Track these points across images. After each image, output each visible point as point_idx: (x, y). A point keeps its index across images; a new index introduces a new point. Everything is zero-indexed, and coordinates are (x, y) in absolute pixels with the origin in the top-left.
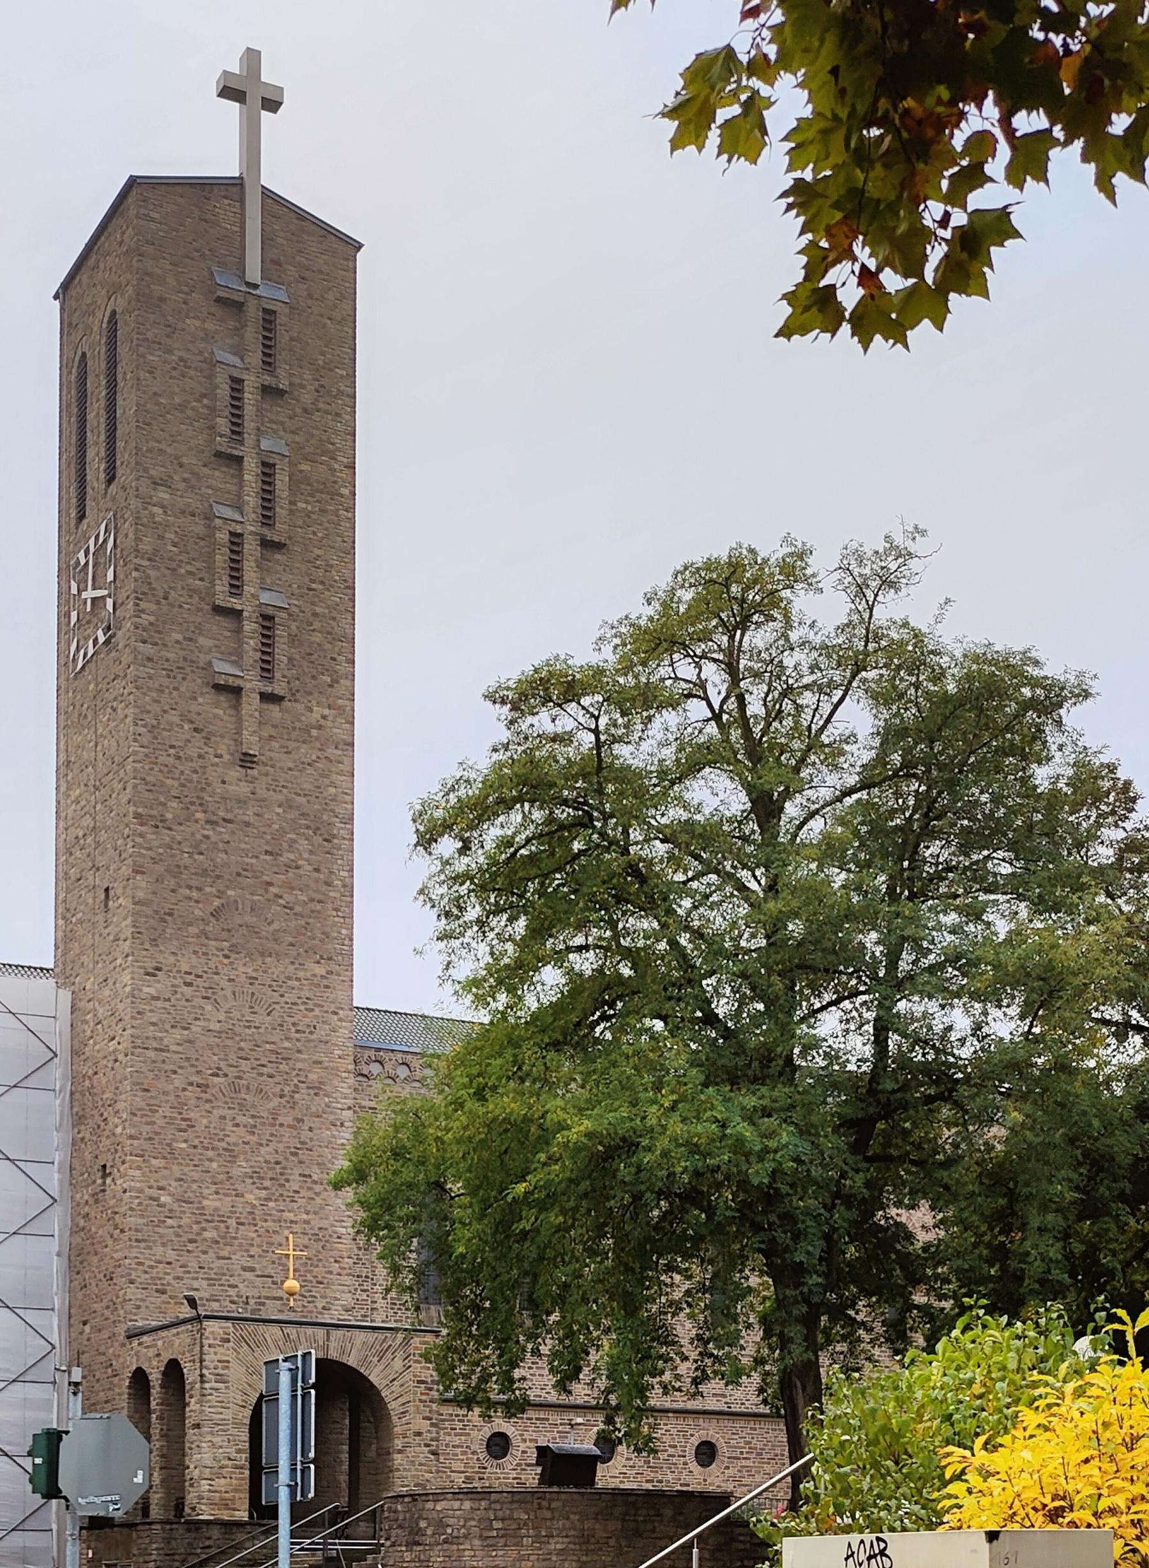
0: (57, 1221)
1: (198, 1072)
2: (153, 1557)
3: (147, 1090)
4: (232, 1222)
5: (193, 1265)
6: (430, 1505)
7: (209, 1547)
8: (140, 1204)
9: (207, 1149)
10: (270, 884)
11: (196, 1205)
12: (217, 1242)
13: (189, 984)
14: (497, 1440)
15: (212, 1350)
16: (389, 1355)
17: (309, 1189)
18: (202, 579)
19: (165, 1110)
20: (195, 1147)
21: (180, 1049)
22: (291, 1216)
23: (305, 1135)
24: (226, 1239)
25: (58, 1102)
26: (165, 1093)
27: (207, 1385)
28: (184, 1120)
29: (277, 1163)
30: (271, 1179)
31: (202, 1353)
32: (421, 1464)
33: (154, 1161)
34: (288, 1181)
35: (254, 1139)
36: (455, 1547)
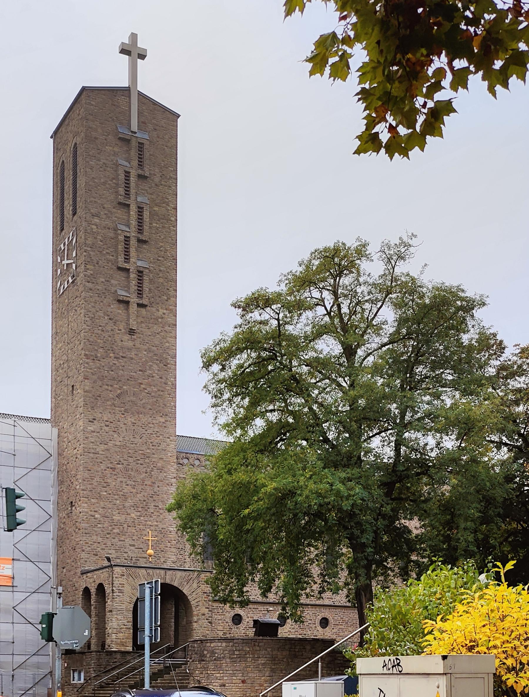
0: (52, 525)
1: (111, 463)
2: (92, 666)
3: (90, 470)
4: (125, 526)
5: (109, 544)
6: (208, 644)
7: (116, 662)
8: (87, 518)
9: (115, 495)
10: (141, 384)
12: (119, 534)
14: (237, 617)
15: (117, 579)
16: (191, 581)
17: (158, 512)
18: (113, 256)
19: (97, 479)
20: (110, 494)
21: (103, 453)
22: (150, 523)
23: (156, 489)
24: (122, 533)
25: (52, 475)
26: (97, 472)
27: (115, 594)
28: (105, 483)
29: (144, 501)
30: (142, 508)
31: (113, 580)
32: (205, 627)
33: (92, 500)
34: (149, 508)
35: (134, 491)
36: (219, 662)
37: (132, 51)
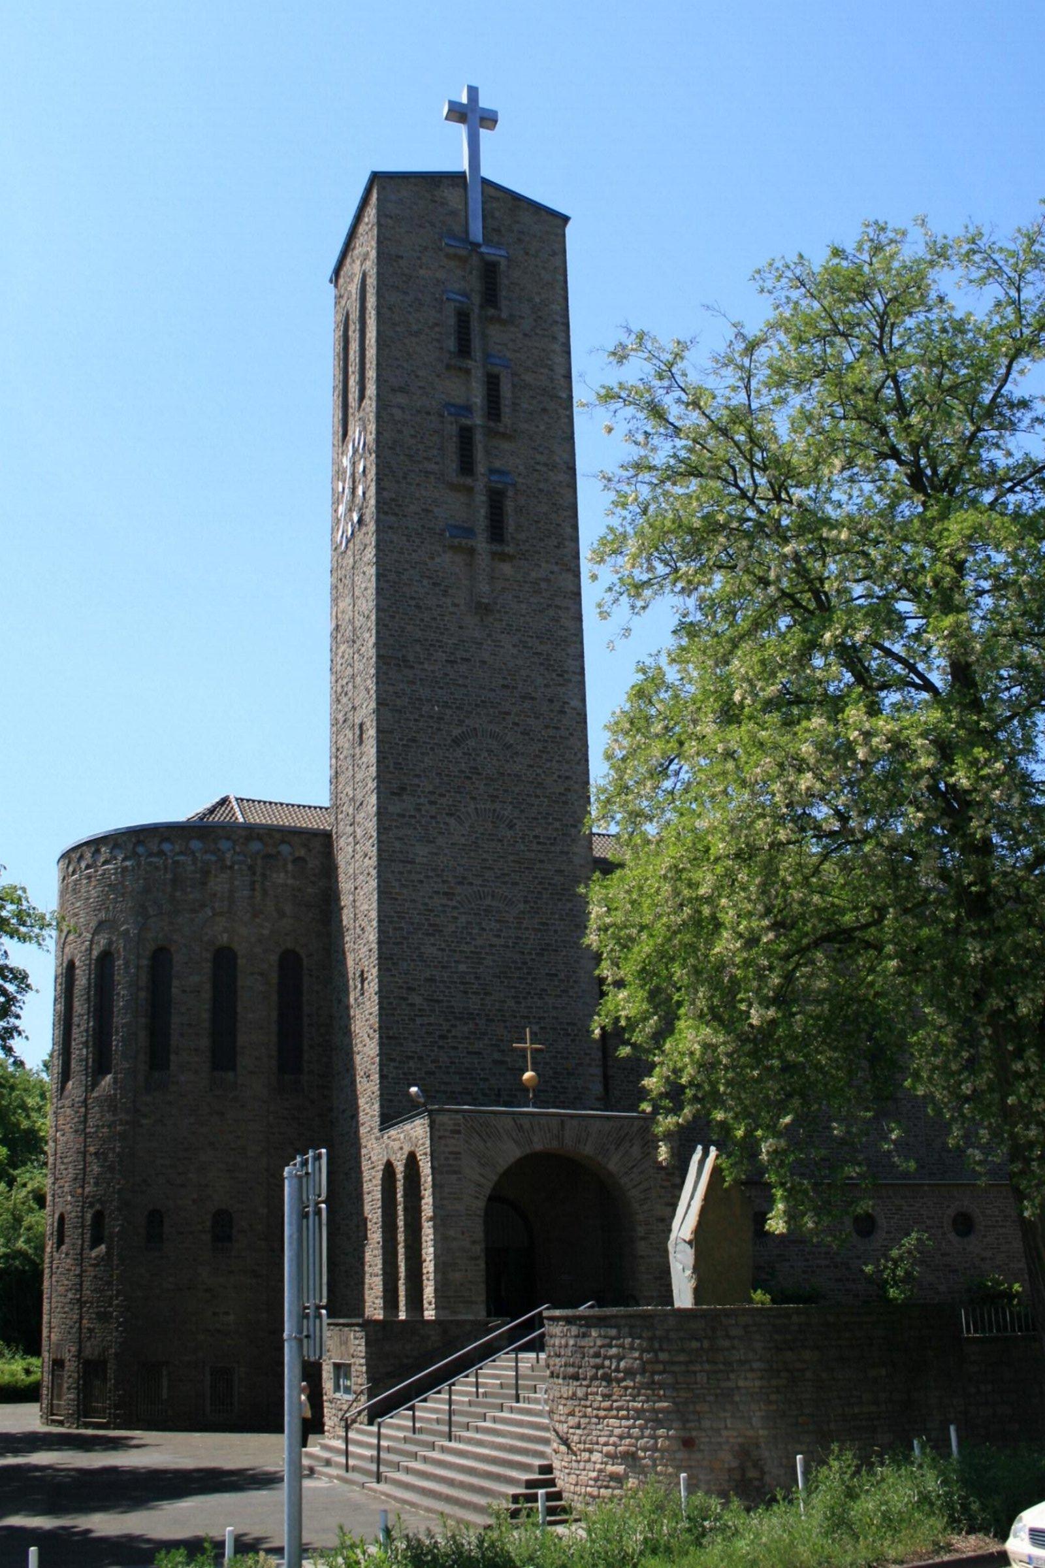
10: (508, 713)
11: (445, 1004)
13: (431, 803)
37: (472, 115)
